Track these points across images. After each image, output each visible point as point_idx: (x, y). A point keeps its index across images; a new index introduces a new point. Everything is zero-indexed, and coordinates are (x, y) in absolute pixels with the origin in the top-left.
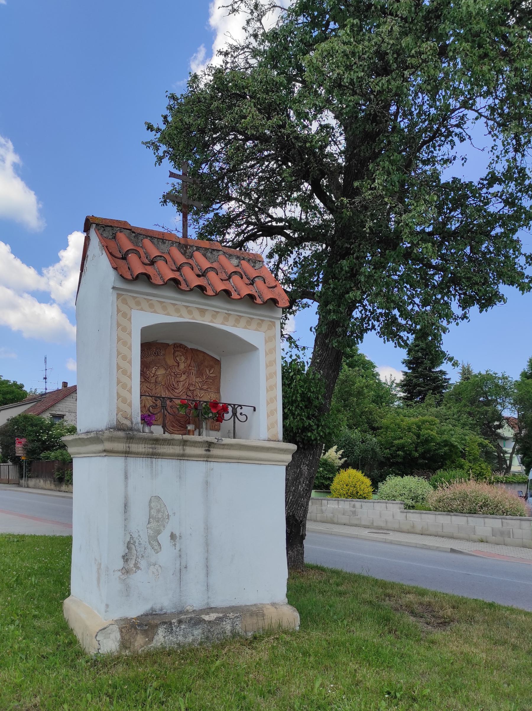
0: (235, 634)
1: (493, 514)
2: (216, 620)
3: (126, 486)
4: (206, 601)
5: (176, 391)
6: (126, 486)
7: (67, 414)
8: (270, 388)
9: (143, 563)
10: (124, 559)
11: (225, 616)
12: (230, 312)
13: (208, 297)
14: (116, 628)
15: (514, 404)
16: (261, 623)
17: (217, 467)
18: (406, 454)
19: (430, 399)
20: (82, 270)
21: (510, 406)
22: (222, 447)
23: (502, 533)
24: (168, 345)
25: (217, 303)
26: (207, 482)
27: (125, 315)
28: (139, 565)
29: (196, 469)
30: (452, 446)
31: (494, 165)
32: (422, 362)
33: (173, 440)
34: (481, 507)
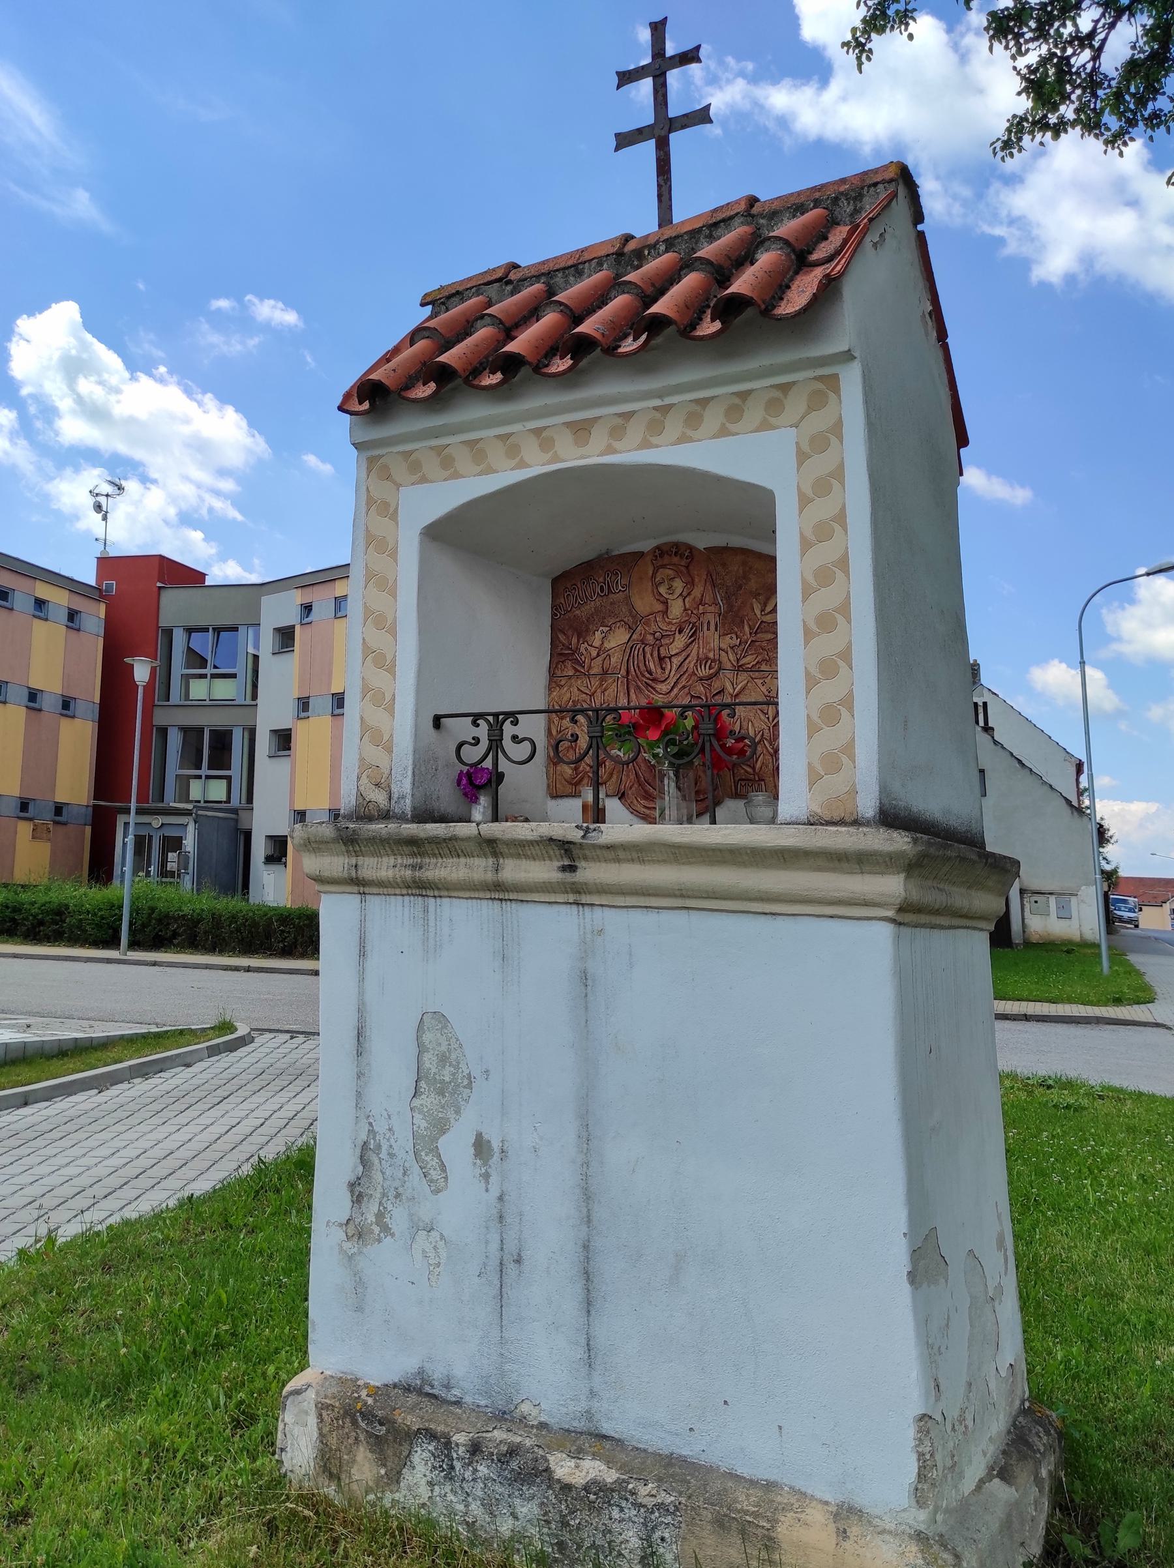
2: (586, 1488)
3: (362, 980)
4: (583, 1405)
5: (659, 687)
6: (362, 980)
9: (398, 1218)
10: (352, 1192)
12: (668, 400)
22: (610, 854)
24: (641, 555)
26: (585, 978)
28: (387, 1220)
33: (454, 838)
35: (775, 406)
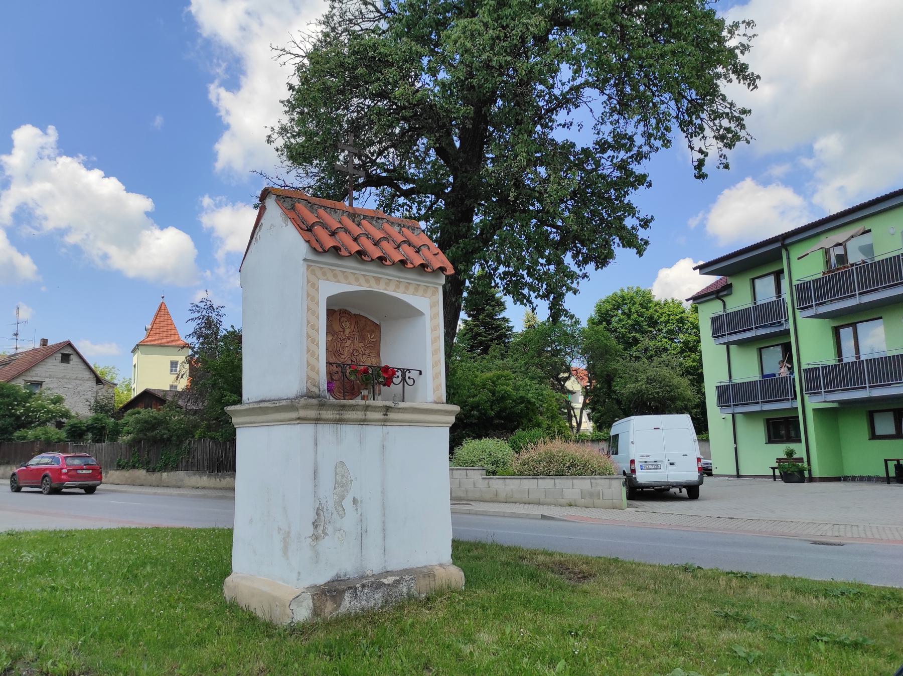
0: (410, 597)
1: (581, 474)
3: (316, 453)
6: (316, 453)
7: (47, 380)
8: (435, 352)
9: (330, 529)
11: (402, 579)
13: (341, 257)
14: (308, 596)
15: (583, 354)
16: (432, 583)
17: (392, 430)
18: (481, 413)
19: (494, 350)
20: (252, 238)
21: (579, 356)
23: (591, 495)
25: (351, 263)
27: (313, 285)
29: (374, 433)
30: (529, 402)
31: (599, 127)
32: (483, 309)
34: (569, 468)
35: (425, 291)
